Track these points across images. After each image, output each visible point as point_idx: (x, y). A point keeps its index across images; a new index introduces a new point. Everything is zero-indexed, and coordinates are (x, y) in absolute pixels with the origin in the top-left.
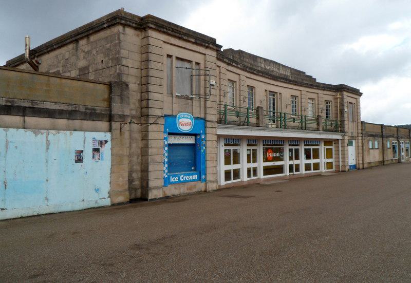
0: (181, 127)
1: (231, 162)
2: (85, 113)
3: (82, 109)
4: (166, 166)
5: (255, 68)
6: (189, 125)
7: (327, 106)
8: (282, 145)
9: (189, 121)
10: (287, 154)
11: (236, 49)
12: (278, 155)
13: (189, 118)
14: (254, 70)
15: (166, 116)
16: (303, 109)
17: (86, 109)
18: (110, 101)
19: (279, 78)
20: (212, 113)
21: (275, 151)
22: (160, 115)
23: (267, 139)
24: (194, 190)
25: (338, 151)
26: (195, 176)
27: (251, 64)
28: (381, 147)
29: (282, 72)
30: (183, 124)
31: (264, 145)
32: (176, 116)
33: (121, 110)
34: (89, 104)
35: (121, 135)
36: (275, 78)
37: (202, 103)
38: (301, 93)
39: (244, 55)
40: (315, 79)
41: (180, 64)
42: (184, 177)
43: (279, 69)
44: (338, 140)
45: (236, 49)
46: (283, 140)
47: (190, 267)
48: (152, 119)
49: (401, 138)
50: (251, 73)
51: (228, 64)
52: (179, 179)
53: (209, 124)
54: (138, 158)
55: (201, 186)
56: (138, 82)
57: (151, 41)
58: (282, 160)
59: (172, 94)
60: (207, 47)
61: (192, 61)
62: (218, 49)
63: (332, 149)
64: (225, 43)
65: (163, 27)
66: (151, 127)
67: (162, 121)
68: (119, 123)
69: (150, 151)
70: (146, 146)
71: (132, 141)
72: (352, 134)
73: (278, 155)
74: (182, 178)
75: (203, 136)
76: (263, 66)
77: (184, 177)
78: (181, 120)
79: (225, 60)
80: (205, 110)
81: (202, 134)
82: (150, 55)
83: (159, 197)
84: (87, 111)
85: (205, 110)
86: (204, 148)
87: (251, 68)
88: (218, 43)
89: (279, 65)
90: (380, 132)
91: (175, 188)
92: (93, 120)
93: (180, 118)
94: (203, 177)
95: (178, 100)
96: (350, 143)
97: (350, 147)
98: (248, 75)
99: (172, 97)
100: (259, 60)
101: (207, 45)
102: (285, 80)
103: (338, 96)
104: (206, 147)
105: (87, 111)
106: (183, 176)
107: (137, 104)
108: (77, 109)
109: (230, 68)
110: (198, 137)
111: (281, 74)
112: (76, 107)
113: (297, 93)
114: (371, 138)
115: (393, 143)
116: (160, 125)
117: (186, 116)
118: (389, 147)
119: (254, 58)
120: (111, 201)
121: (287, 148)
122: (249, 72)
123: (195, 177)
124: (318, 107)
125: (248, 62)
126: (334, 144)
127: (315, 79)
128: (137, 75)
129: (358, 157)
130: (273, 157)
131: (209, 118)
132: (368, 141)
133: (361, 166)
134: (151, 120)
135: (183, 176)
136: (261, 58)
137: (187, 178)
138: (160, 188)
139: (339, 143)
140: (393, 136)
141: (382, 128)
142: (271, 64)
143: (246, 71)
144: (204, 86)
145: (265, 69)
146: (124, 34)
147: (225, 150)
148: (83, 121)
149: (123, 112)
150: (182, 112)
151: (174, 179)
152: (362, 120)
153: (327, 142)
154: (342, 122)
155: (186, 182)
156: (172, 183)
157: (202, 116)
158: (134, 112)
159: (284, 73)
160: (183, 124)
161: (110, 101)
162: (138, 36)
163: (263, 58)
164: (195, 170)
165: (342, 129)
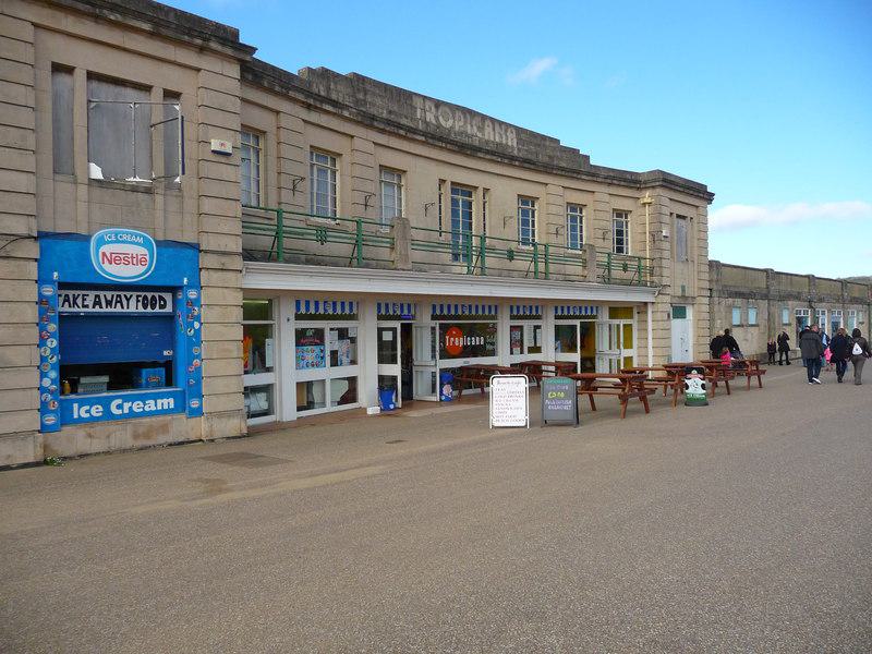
0: (106, 266)
1: (576, 347)
4: (54, 374)
5: (404, 121)
6: (140, 262)
7: (620, 224)
8: (594, 317)
9: (142, 251)
10: (503, 339)
11: (344, 72)
12: (478, 341)
14: (400, 126)
19: (480, 150)
21: (470, 331)
22: (23, 231)
23: (487, 304)
26: (165, 401)
27: (390, 112)
28: (763, 323)
29: (490, 135)
31: (557, 318)
32: (87, 238)
39: (548, 143)
40: (587, 158)
43: (481, 129)
44: (646, 303)
45: (343, 68)
46: (495, 304)
49: (821, 300)
50: (391, 134)
51: (309, 107)
58: (493, 353)
60: (202, 50)
61: (151, 87)
62: (241, 56)
63: (624, 325)
64: (284, 52)
65: (671, 182)
72: (683, 290)
73: (478, 341)
74: (119, 407)
76: (430, 117)
77: (127, 406)
78: (107, 249)
79: (291, 93)
81: (190, 286)
87: (389, 122)
88: (243, 40)
89: (484, 117)
93: (101, 242)
96: (679, 312)
97: (676, 323)
98: (568, 183)
100: (418, 103)
101: (199, 41)
102: (499, 155)
106: (119, 401)
109: (314, 117)
110: (180, 296)
111: (487, 142)
113: (529, 190)
114: (739, 301)
115: (799, 312)
118: (786, 320)
121: (504, 326)
122: (383, 131)
126: (636, 316)
127: (587, 158)
130: (465, 347)
132: (730, 308)
136: (425, 97)
137: (137, 407)
139: (646, 312)
140: (797, 297)
141: (768, 277)
142: (458, 114)
143: (370, 126)
145: (439, 126)
150: (112, 226)
151: (88, 411)
152: (710, 258)
153: (617, 310)
155: (132, 414)
156: (80, 420)
163: (430, 99)
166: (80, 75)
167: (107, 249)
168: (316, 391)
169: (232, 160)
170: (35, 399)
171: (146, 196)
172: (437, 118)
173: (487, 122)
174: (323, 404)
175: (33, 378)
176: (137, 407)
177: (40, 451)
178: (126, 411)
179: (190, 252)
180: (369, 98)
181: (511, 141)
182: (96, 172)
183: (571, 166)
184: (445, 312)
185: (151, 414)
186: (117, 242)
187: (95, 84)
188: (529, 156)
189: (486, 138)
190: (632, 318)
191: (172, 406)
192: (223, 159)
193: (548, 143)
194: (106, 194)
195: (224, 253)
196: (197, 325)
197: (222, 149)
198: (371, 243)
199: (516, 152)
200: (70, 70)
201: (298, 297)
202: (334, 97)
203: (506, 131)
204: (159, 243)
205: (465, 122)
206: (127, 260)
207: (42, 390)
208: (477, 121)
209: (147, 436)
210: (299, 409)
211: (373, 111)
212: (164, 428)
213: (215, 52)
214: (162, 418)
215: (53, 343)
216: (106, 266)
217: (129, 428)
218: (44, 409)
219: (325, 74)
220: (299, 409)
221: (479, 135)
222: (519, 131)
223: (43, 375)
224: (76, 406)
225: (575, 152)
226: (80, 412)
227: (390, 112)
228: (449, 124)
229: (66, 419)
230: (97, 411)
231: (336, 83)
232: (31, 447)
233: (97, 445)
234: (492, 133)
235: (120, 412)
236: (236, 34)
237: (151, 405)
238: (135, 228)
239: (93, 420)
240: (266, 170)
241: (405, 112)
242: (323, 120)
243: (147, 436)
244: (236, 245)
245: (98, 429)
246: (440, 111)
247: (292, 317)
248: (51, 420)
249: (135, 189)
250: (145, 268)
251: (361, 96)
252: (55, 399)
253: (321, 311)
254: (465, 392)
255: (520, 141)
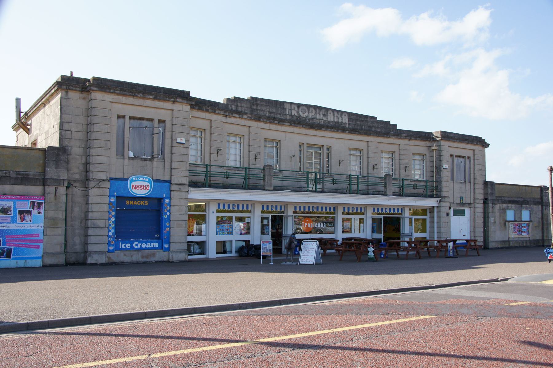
0: (134, 190)
2: (16, 179)
3: (13, 175)
4: (113, 231)
9: (147, 184)
13: (146, 181)
15: (112, 179)
16: (371, 166)
17: (17, 174)
18: (44, 166)
20: (182, 174)
22: (105, 178)
24: (153, 259)
25: (434, 222)
27: (270, 113)
29: (330, 118)
30: (136, 187)
32: (127, 180)
33: (56, 174)
34: (21, 170)
35: (55, 199)
36: (319, 127)
37: (167, 164)
38: (368, 144)
39: (369, 120)
40: (395, 126)
41: (136, 123)
42: (139, 245)
45: (246, 96)
47: (479, 349)
48: (93, 182)
52: (132, 246)
53: (174, 187)
54: (81, 222)
55: (161, 255)
56: (83, 146)
57: (95, 104)
59: (123, 155)
66: (92, 192)
67: (107, 185)
68: (54, 187)
69: (90, 215)
70: (87, 212)
71: (74, 205)
74: (137, 245)
75: (167, 201)
76: (294, 113)
77: (139, 245)
78: (134, 183)
80: (400, 157)
81: (166, 198)
82: (93, 118)
83: (100, 262)
84: (19, 176)
85: (400, 157)
86: (168, 214)
89: (327, 109)
90: (539, 197)
91: (125, 255)
92: (25, 185)
93: (132, 181)
94: (166, 246)
95: (132, 161)
96: (459, 213)
99: (124, 159)
100: (288, 106)
103: (433, 148)
104: (170, 213)
105: (19, 176)
106: (137, 243)
107: (81, 168)
108: (7, 175)
111: (329, 122)
112: (6, 174)
116: (104, 189)
117: (141, 179)
119: (279, 105)
120: (43, 262)
123: (156, 245)
124: (400, 162)
125: (265, 111)
126: (428, 214)
127: (395, 126)
128: (81, 138)
129: (474, 232)
131: (175, 180)
133: (480, 243)
134: (92, 184)
135: (137, 243)
136: (291, 103)
137: (143, 245)
138: (103, 253)
144: (170, 145)
145: (299, 116)
146: (66, 99)
147: (218, 217)
148: (14, 186)
149: (59, 176)
151: (125, 246)
154: (439, 182)
155: (141, 249)
156: (122, 249)
157: (167, 178)
158: (77, 176)
159: (336, 120)
160: (136, 187)
161: (44, 166)
162: (84, 99)
163: (294, 104)
164: (158, 238)
165: (438, 193)
166: (127, 118)
167: (134, 183)
168: (228, 245)
169: (185, 146)
170: (105, 240)
171: (150, 162)
172: (298, 112)
173: (330, 112)
174: (231, 252)
175: (105, 232)
176: (143, 245)
177: (107, 259)
178: (139, 247)
179: (167, 184)
180: (259, 108)
181: (345, 120)
182: (131, 154)
183: (387, 130)
184: (226, 208)
185: (149, 249)
186: (138, 180)
187: (132, 121)
188: (356, 127)
189: (329, 120)
190: (426, 215)
191: (157, 246)
192: (182, 145)
193: (369, 120)
194: (135, 162)
195: (181, 185)
196: (168, 214)
197: (181, 142)
198: (326, 165)
199: (347, 126)
200: (124, 117)
201: (219, 203)
202: (240, 109)
203: (342, 115)
204: (154, 181)
205: (316, 113)
206: (142, 187)
207: (109, 236)
208: (323, 112)
209: (147, 257)
210: (217, 253)
211: (261, 113)
212: (154, 255)
213: (179, 102)
214: (152, 251)
215: (113, 219)
216: (134, 190)
217: (140, 254)
218: (109, 244)
219: (236, 100)
220: (217, 253)
221: (324, 119)
222: (350, 114)
223: (109, 231)
224: (121, 243)
225: (387, 123)
226: (122, 246)
227: (270, 113)
228: (305, 115)
229: (117, 248)
230: (128, 246)
231: (241, 103)
232: (104, 257)
233: (126, 259)
234: (332, 117)
235: (136, 247)
236: (189, 93)
237: (149, 245)
238: (145, 175)
239: (126, 249)
240: (205, 146)
241: (279, 112)
242: (233, 120)
243: (147, 257)
244: (186, 181)
245: (127, 253)
246: (300, 110)
247: (215, 211)
248: (111, 248)
249: (145, 159)
250: (147, 191)
251: (255, 107)
252: (113, 240)
253: (231, 208)
254: (328, 251)
255: (350, 119)
